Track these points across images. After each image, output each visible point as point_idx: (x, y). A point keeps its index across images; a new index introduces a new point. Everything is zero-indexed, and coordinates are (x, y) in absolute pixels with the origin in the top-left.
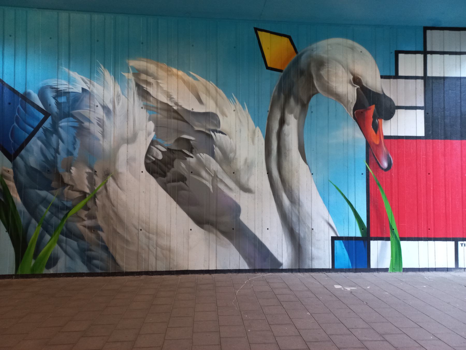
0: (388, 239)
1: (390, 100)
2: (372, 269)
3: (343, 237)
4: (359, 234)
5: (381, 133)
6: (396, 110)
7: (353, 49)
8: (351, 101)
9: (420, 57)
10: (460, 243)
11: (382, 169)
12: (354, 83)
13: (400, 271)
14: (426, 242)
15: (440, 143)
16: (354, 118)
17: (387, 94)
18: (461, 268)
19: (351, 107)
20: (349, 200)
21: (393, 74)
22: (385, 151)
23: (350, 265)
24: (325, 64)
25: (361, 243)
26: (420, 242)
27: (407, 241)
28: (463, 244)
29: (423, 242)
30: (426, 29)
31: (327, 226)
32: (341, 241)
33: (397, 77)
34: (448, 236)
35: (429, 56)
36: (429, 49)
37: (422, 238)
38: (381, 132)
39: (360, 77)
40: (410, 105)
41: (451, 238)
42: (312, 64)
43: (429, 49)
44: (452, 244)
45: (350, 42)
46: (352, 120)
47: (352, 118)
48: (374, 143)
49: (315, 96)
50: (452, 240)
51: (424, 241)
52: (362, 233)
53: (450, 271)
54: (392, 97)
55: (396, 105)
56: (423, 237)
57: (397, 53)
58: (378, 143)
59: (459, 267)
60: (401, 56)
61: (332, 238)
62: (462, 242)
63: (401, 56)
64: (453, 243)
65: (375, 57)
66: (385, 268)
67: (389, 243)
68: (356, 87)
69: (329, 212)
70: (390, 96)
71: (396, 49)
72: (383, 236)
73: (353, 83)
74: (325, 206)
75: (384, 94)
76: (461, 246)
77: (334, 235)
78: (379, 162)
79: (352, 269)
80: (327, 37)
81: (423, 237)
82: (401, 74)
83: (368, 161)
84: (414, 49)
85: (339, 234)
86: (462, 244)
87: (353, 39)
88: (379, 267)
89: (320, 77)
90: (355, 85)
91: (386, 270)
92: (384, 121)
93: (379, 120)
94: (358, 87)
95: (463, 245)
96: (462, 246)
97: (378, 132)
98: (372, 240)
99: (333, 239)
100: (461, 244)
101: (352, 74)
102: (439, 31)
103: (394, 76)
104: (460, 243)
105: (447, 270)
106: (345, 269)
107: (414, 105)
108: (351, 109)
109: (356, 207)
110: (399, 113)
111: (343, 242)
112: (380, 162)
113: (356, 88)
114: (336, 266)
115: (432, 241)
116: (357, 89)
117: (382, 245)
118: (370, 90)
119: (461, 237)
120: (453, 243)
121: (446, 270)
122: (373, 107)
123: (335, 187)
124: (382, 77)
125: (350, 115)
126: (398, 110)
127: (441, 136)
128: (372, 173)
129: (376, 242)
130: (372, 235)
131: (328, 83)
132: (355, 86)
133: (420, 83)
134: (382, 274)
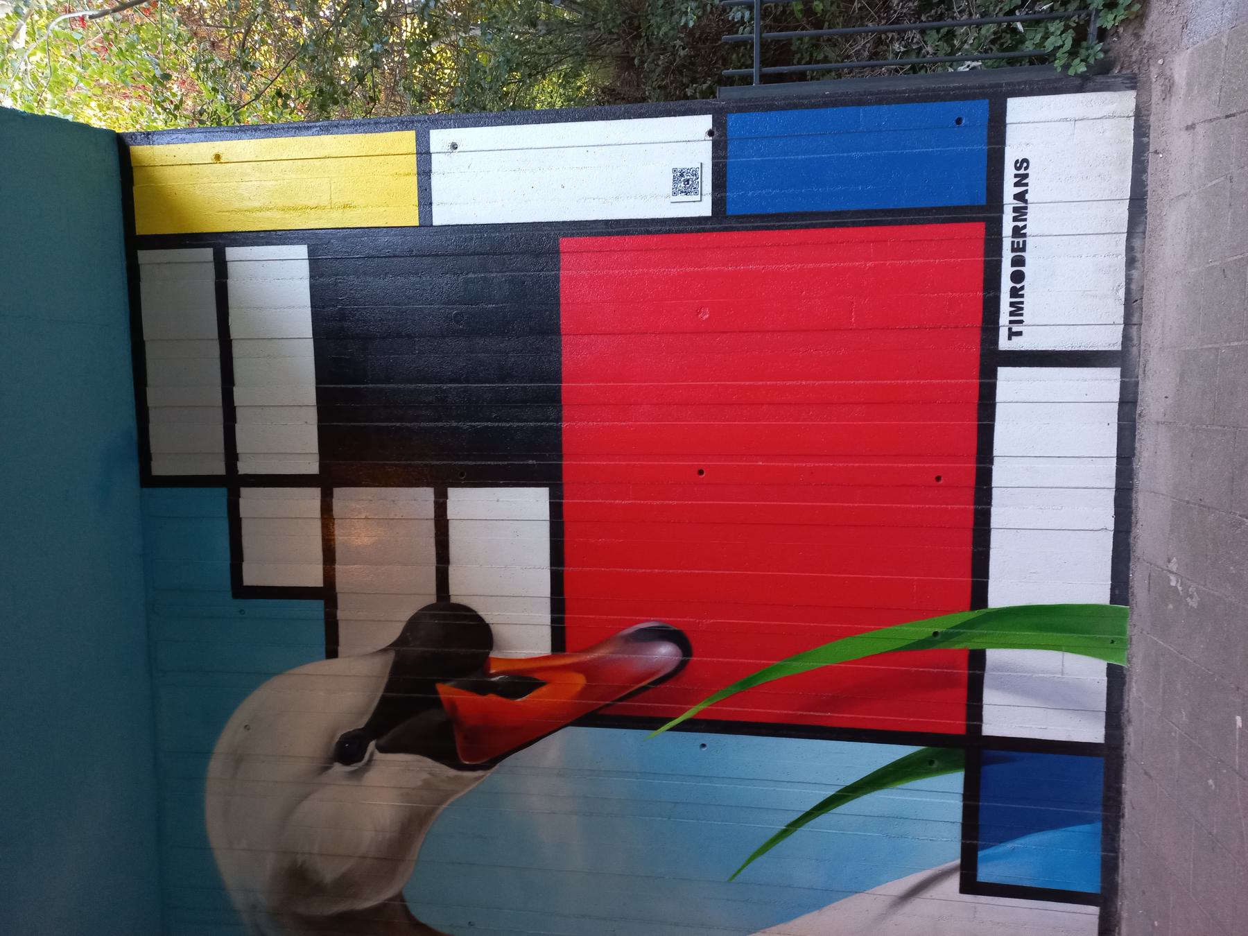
0: (977, 660)
1: (413, 624)
2: (1107, 736)
3: (962, 844)
4: (954, 781)
5: (543, 664)
6: (454, 600)
7: (239, 759)
8: (425, 776)
9: (251, 499)
10: (1004, 344)
11: (682, 666)
12: (360, 760)
13: (1123, 616)
14: (995, 492)
15: (573, 425)
16: (485, 767)
17: (394, 632)
18: (1126, 338)
19: (449, 778)
20: (808, 808)
21: (318, 607)
22: (607, 651)
23: (1086, 828)
24: (299, 864)
25: (993, 773)
26: (995, 521)
27: (1000, 292)
28: (1010, 329)
29: (994, 510)
30: (148, 480)
31: (918, 905)
32: (981, 854)
33: (327, 594)
34: (974, 394)
35: (244, 468)
36: (219, 469)
37: (976, 512)
38: (534, 665)
39: (337, 740)
40: (432, 541)
41: (978, 469)
42: (302, 909)
43: (219, 469)
44: (1008, 380)
45: (216, 767)
46: (501, 776)
47: (488, 773)
48: (583, 693)
49: (411, 906)
50: (991, 378)
51: (990, 504)
52: (948, 767)
53: (1136, 393)
54: (406, 614)
55: (432, 599)
56: (972, 507)
57: (241, 591)
58: (580, 680)
59: (1119, 348)
60: (251, 577)
61: (965, 889)
62: (1003, 333)
63: (251, 577)
64: (1005, 375)
65: (263, 676)
66: (1109, 682)
67: (994, 656)
68: (372, 755)
69: (856, 893)
70: (400, 621)
71: (230, 594)
72: (965, 679)
73: (360, 764)
74: (836, 903)
75: (394, 645)
76: (1019, 338)
77: (954, 882)
78: (656, 677)
79: (1106, 821)
80: (203, 849)
81: (972, 507)
82: (313, 577)
83: (651, 722)
84: (223, 526)
85: (954, 860)
86: (1012, 334)
87: (205, 753)
88: (1103, 706)
89: (346, 886)
90: (367, 756)
91: (1116, 678)
92: (494, 648)
93: (493, 671)
94: (372, 745)
95: (1016, 328)
96: (1019, 334)
97: (538, 676)
98: (979, 728)
99: (970, 885)
100: (1010, 338)
101: (325, 769)
102: (152, 427)
103: (326, 606)
104: (1004, 344)
105: (1128, 403)
106: (1104, 850)
107: (430, 526)
108: (456, 777)
109: (837, 783)
110: (459, 591)
111: (985, 847)
112: (657, 672)
113: (378, 755)
114: (1092, 885)
115: (994, 468)
116: (383, 749)
117: (1004, 686)
118: (384, 701)
119: (976, 337)
120: (1005, 375)
121: (1127, 408)
122: (446, 690)
123: (759, 859)
124: (332, 652)
125: (477, 783)
126: (451, 592)
127: (547, 420)
128: (701, 706)
129: (988, 713)
130: (956, 724)
131: (363, 857)
132: (370, 760)
133: (344, 498)
134: (1135, 692)
